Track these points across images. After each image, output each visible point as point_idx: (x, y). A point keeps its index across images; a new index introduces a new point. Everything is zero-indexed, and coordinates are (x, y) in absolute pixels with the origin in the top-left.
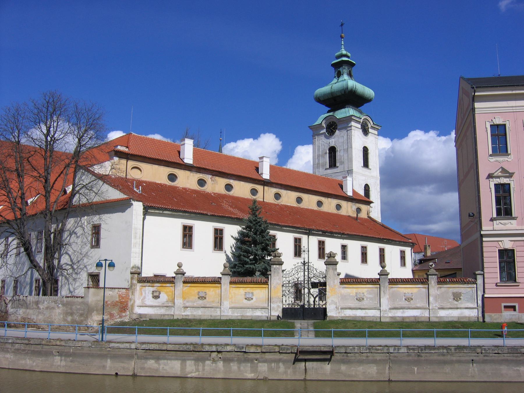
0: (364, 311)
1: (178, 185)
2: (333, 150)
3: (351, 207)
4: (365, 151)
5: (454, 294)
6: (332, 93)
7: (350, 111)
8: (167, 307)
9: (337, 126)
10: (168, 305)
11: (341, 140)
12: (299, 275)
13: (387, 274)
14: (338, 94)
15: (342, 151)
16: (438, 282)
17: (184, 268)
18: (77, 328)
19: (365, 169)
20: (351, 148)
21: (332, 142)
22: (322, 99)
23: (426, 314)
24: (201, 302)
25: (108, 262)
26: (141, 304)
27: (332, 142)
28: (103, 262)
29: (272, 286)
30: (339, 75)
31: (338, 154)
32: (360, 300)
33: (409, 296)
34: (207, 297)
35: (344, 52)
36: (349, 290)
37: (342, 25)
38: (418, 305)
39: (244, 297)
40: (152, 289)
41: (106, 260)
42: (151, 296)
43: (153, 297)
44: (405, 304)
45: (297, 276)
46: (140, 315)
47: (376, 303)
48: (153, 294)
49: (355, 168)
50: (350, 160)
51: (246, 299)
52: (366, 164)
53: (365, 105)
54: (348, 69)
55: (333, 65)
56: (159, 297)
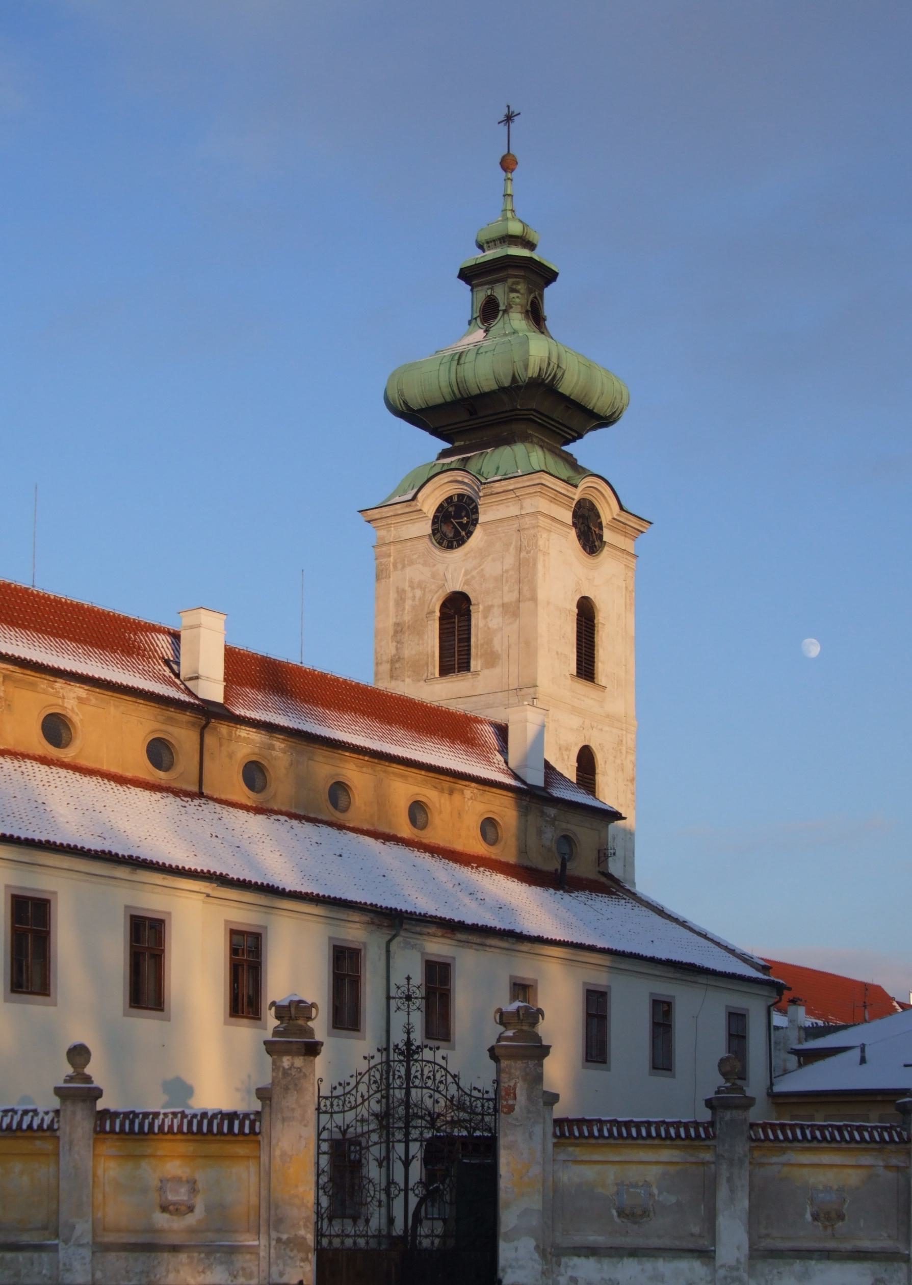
2: (456, 610)
3: (540, 833)
4: (586, 614)
9: (475, 511)
11: (492, 568)
15: (496, 611)
18: (246, 836)
19: (582, 686)
20: (534, 599)
21: (456, 569)
27: (456, 569)
31: (478, 621)
32: (633, 1215)
37: (509, 118)
38: (866, 1244)
49: (544, 682)
50: (528, 645)
52: (586, 668)
54: (530, 291)
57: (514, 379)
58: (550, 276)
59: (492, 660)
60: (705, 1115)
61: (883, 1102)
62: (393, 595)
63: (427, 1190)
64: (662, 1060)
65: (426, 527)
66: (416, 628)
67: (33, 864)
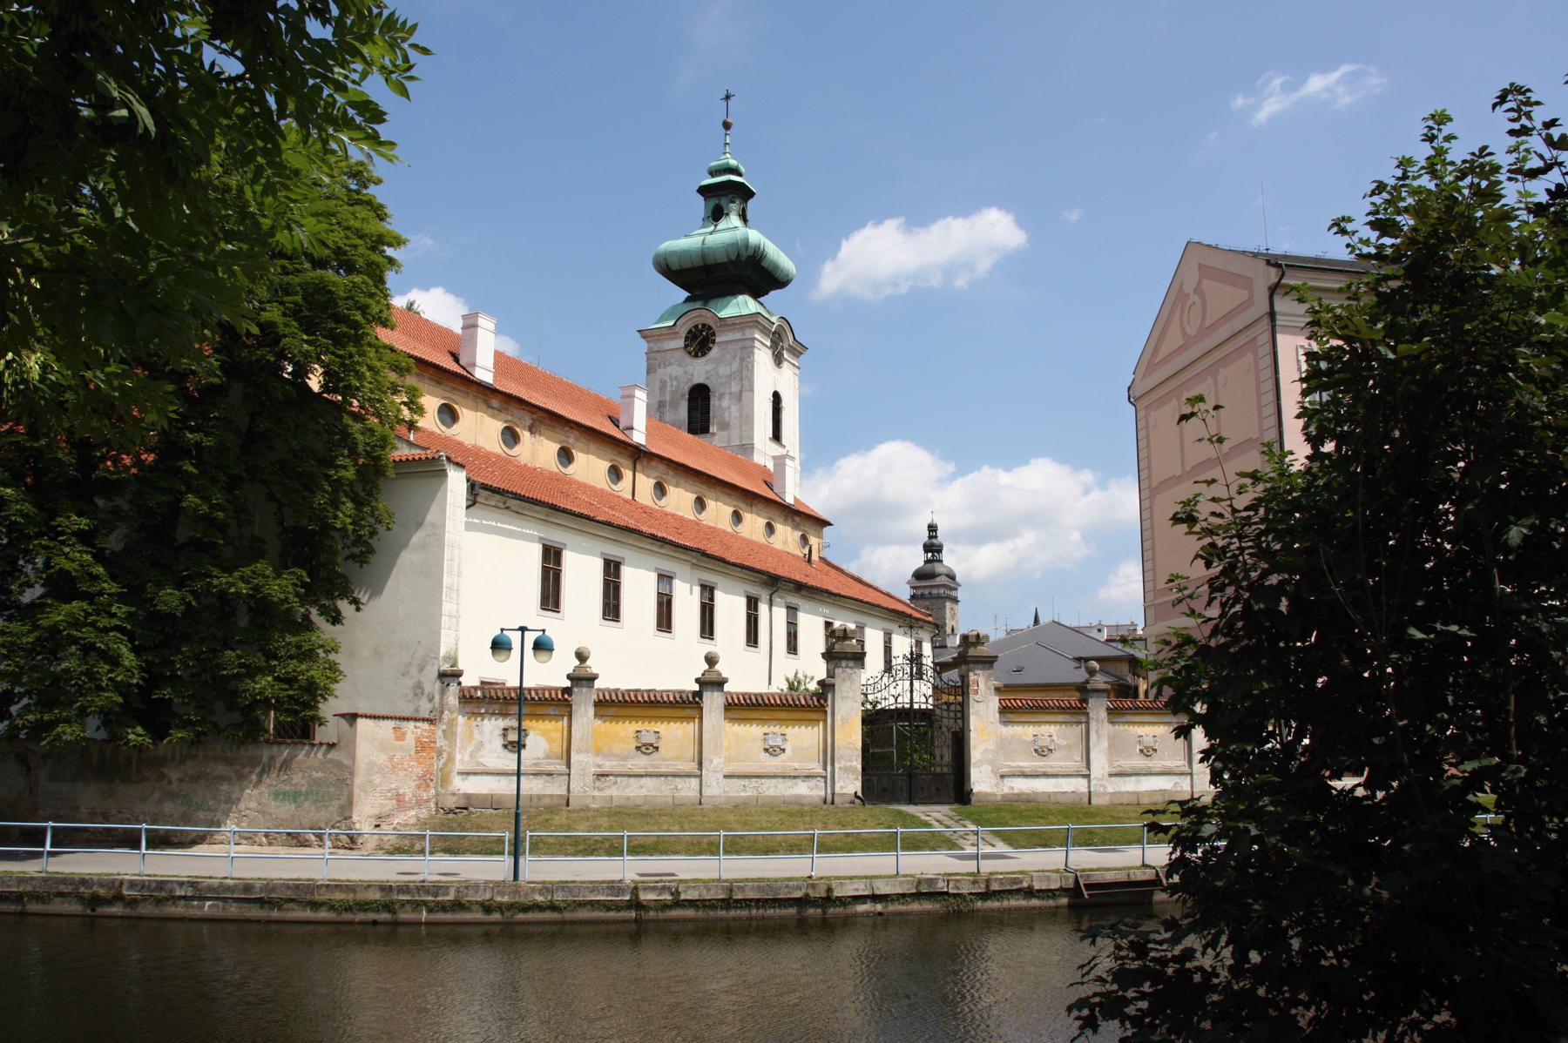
0: (1053, 781)
1: (459, 438)
6: (704, 253)
7: (743, 305)
8: (550, 774)
10: (549, 768)
11: (724, 370)
12: (899, 689)
13: (591, 679)
14: (722, 259)
16: (1004, 710)
17: (593, 665)
20: (752, 390)
22: (675, 267)
23: (1080, 785)
24: (640, 763)
25: (530, 638)
26: (470, 768)
27: (698, 370)
28: (515, 638)
29: (838, 717)
30: (717, 215)
32: (1041, 752)
33: (1149, 741)
34: (660, 744)
35: (733, 162)
36: (1018, 729)
37: (727, 97)
39: (761, 745)
40: (501, 723)
41: (523, 629)
42: (499, 742)
43: (505, 746)
44: (1140, 762)
45: (893, 692)
46: (468, 796)
47: (1076, 763)
48: (505, 736)
51: (766, 750)
53: (772, 293)
55: (703, 191)
58: (751, 194)
59: (725, 426)
62: (658, 384)
65: (681, 343)
66: (674, 405)
67: (588, 518)
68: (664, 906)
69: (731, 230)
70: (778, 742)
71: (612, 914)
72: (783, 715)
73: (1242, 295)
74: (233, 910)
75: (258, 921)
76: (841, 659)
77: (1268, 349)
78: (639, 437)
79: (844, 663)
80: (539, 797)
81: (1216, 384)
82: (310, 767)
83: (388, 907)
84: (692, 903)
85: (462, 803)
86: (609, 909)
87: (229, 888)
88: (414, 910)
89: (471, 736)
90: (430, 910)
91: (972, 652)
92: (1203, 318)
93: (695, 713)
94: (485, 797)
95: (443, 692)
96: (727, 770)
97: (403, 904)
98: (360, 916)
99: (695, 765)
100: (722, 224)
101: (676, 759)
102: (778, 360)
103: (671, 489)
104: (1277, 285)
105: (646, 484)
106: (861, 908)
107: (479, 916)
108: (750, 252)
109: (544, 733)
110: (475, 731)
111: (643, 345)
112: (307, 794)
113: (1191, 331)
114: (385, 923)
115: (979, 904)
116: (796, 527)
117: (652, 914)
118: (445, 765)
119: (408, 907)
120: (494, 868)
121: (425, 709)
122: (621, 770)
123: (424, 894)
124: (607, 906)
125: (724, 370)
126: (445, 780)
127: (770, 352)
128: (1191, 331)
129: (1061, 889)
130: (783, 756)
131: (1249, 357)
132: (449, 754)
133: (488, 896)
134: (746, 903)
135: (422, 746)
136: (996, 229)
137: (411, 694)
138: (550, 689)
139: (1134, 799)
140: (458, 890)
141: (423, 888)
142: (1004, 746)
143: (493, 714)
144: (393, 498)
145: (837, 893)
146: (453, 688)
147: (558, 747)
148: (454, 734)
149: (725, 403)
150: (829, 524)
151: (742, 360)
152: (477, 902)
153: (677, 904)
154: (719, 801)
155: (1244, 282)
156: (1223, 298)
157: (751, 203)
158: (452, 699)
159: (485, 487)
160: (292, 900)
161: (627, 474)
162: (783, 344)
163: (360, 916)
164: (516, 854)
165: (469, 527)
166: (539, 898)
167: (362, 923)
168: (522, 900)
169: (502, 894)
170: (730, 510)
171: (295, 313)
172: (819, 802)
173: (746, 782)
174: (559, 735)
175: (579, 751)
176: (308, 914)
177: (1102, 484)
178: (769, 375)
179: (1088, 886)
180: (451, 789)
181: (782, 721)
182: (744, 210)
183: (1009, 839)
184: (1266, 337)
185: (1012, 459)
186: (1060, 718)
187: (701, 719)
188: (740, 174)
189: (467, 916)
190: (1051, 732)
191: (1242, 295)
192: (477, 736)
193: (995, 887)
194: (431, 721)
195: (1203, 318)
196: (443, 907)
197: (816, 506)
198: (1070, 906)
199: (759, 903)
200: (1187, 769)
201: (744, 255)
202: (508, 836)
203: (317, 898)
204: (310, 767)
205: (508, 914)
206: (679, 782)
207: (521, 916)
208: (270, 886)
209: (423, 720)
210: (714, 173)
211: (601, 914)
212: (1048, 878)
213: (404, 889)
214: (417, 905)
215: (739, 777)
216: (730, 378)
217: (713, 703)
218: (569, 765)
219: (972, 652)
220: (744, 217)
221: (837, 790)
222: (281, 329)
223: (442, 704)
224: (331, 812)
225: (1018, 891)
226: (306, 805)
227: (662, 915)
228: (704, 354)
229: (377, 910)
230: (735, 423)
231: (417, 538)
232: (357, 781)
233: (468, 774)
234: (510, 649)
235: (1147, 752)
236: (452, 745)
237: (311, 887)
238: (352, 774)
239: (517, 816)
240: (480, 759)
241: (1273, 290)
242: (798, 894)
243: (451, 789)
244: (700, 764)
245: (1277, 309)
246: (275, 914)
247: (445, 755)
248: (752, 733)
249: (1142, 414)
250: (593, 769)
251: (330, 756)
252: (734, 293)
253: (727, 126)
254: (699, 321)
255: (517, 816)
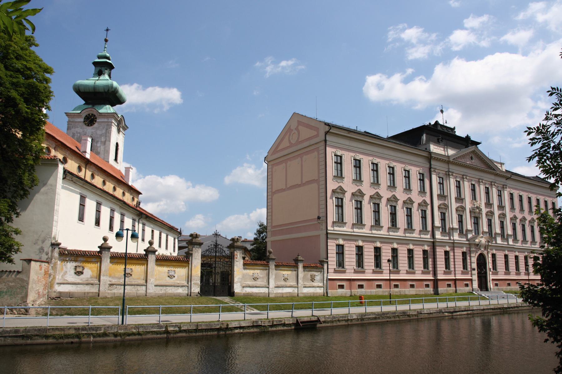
0: (258, 289)
5: (426, 285)
6: (95, 87)
7: (107, 109)
8: (92, 284)
9: (96, 118)
10: (92, 282)
11: (99, 132)
13: (110, 248)
16: (244, 264)
20: (110, 141)
22: (82, 90)
23: (265, 290)
26: (61, 281)
29: (193, 265)
30: (100, 73)
32: (255, 279)
33: (286, 276)
34: (132, 273)
35: (108, 55)
37: (107, 30)
39: (167, 275)
40: (74, 264)
42: (73, 271)
43: (75, 273)
44: (283, 283)
46: (60, 293)
47: (264, 283)
48: (75, 269)
51: (169, 276)
55: (95, 64)
56: (82, 273)
57: (108, 90)
60: (99, 250)
61: (370, 315)
63: (268, 262)
64: (167, 248)
65: (82, 120)
68: (176, 332)
69: (104, 80)
70: (172, 273)
71: (159, 336)
72: (175, 264)
73: (315, 133)
74: (9, 341)
75: (21, 345)
76: (195, 245)
77: (323, 151)
78: (88, 156)
79: (196, 246)
80: (88, 293)
81: (302, 160)
82: (9, 281)
83: (78, 336)
84: (185, 331)
85: (58, 295)
86: (157, 334)
87: (7, 332)
88: (88, 337)
89: (62, 269)
90: (94, 337)
91: (236, 244)
92: (298, 138)
93: (145, 262)
94: (67, 293)
95: (52, 251)
96: (156, 284)
97: (84, 335)
98: (66, 341)
99: (144, 281)
100: (102, 77)
101: (138, 279)
102: (119, 131)
103: (96, 177)
104: (328, 132)
105: (89, 173)
106: (237, 331)
107: (113, 338)
108: (113, 90)
109: (90, 268)
110: (64, 267)
111: (66, 119)
112: (6, 292)
113: (293, 142)
114: (76, 343)
115: (270, 329)
116: (131, 194)
117: (172, 335)
118: (52, 280)
119: (85, 336)
120: (113, 320)
121: (44, 257)
122: (118, 283)
123: (42, 332)
124: (157, 333)
125: (99, 132)
126: (51, 286)
127: (116, 128)
128: (293, 142)
129: (293, 323)
130: (174, 279)
131: (316, 153)
132: (54, 276)
133: (116, 331)
134: (202, 330)
135: (46, 273)
136: (174, 95)
137: (38, 252)
138: (93, 252)
139: (281, 295)
140: (105, 329)
141: (92, 328)
142: (244, 276)
143: (71, 260)
144: (39, 172)
145: (230, 326)
146: (57, 250)
147: (95, 274)
148: (56, 268)
149: (99, 145)
150: (141, 194)
151: (107, 129)
152: (112, 333)
153: (181, 331)
154: (152, 295)
155: (317, 129)
156: (306, 133)
157: (113, 71)
158: (56, 254)
159: (69, 172)
160: (37, 335)
161: (83, 169)
162: (122, 126)
163: (66, 341)
164: (123, 314)
165: (63, 188)
166: (134, 331)
167: (67, 343)
168: (128, 331)
169: (121, 329)
170: (113, 186)
171: (22, 95)
172: (185, 295)
173: (162, 288)
174: (96, 269)
175: (104, 276)
176: (44, 341)
177: (194, 187)
178: (116, 137)
179: (302, 322)
180: (54, 290)
181: (174, 266)
182: (110, 73)
183: (256, 307)
184: (323, 147)
185: (163, 173)
186: (261, 268)
187: (147, 264)
188: (109, 60)
189: (108, 338)
190: (286, 273)
191: (315, 133)
192: (64, 269)
193: (275, 323)
194: (48, 262)
195: (298, 138)
196: (99, 335)
197: (137, 186)
198: (295, 329)
199: (206, 330)
200: (296, 286)
201: (111, 90)
202: (120, 307)
203: (48, 334)
204: (9, 281)
205: (123, 337)
206: (139, 288)
207: (128, 338)
208: (26, 330)
209: (45, 262)
210: (99, 57)
211: (155, 336)
212: (289, 320)
213: (84, 329)
214: (89, 335)
215: (159, 286)
216: (101, 135)
217: (152, 258)
218: (99, 281)
219: (236, 244)
220: (110, 76)
221: (192, 291)
222: (18, 101)
223: (52, 256)
224: (18, 299)
225: (281, 324)
226: (6, 297)
227: (175, 335)
228: (91, 125)
229: (73, 338)
230: (102, 152)
231: (43, 190)
232: (30, 286)
233: (61, 284)
234: (123, 237)
235: (285, 280)
236: (55, 272)
237: (45, 329)
238: (28, 284)
239: (124, 300)
240: (68, 279)
241: (326, 133)
242: (218, 327)
243: (54, 290)
244: (146, 281)
245: (327, 139)
246: (29, 341)
247: (52, 276)
248: (164, 270)
249: (270, 167)
250: (109, 282)
251: (18, 276)
252: (105, 104)
253: (106, 41)
254: (91, 113)
255: (124, 300)
